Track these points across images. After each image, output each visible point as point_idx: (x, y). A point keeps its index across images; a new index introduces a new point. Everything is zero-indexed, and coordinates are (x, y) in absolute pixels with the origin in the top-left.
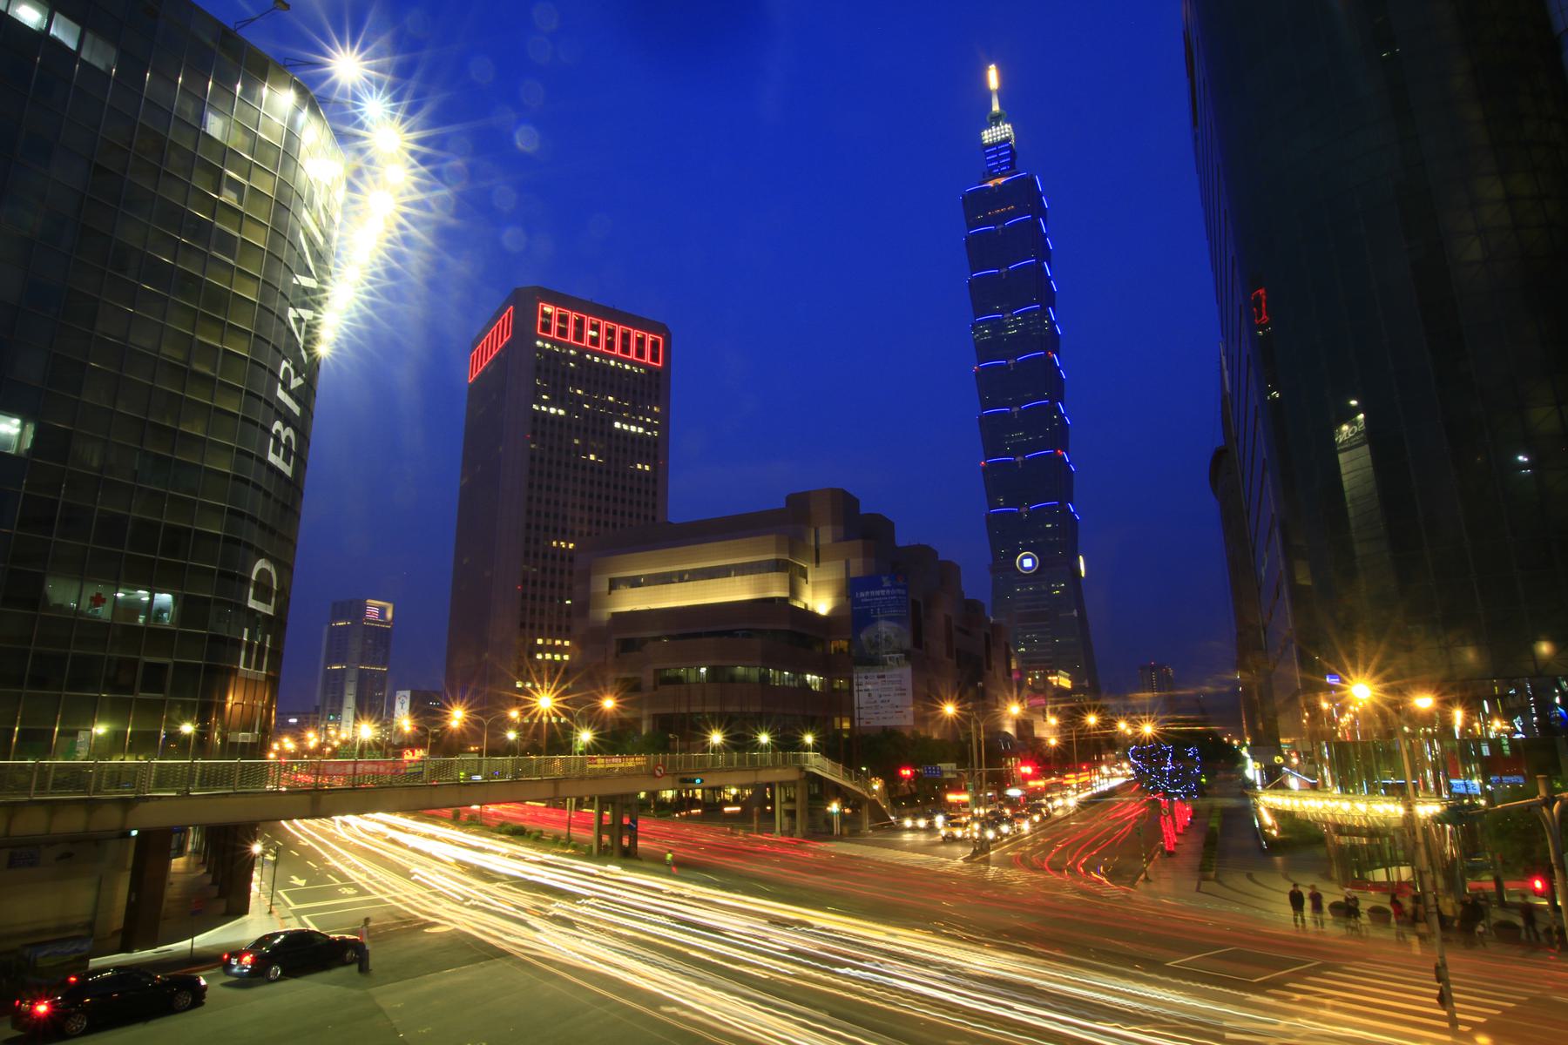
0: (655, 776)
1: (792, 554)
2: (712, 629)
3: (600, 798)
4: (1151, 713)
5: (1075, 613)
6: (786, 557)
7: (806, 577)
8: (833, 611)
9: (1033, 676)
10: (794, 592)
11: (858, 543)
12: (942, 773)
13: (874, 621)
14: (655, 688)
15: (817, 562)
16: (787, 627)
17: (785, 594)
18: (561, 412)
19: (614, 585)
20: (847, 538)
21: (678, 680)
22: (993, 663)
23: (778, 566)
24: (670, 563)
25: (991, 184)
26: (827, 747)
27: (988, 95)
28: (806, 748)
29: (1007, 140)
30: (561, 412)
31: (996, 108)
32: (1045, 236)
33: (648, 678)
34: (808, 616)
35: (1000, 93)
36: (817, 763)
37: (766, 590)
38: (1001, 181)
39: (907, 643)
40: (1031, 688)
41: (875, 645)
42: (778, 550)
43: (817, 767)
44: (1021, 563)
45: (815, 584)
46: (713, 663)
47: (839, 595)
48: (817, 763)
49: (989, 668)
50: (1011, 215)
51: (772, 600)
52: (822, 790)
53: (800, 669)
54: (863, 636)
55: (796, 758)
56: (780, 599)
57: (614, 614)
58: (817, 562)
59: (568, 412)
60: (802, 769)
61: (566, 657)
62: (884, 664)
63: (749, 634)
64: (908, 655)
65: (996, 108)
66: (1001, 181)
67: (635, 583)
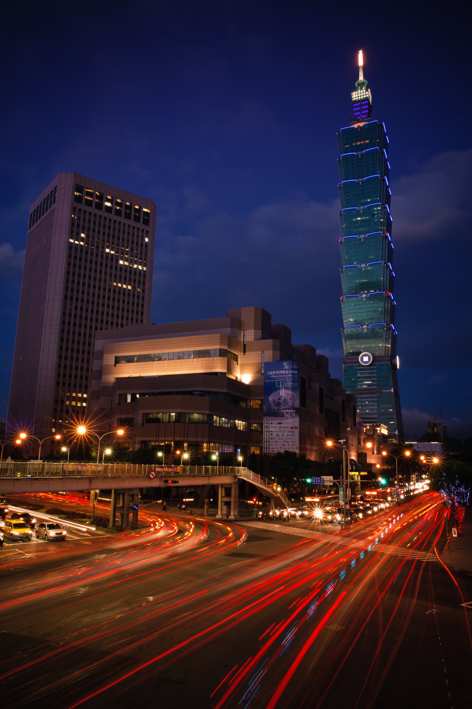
0: (150, 478)
1: (229, 346)
2: (180, 390)
3: (115, 490)
4: (423, 466)
5: (392, 390)
6: (226, 348)
7: (237, 360)
8: (253, 382)
9: (366, 427)
10: (230, 369)
11: (270, 342)
12: (324, 481)
13: (279, 389)
14: (143, 425)
15: (244, 352)
16: (225, 391)
17: (224, 371)
18: (129, 287)
19: (118, 360)
20: (263, 338)
21: (157, 421)
22: (346, 418)
23: (223, 353)
24: (154, 348)
25: (356, 126)
26: (251, 463)
27: (357, 69)
28: (238, 464)
29: (367, 99)
30: (129, 287)
31: (361, 78)
32: (385, 134)
33: (139, 419)
34: (238, 384)
35: (364, 68)
36: (245, 474)
37: (211, 367)
38: (361, 124)
39: (297, 404)
40: (366, 434)
41: (279, 404)
42: (221, 344)
43: (245, 476)
44: (362, 359)
45: (243, 366)
46: (179, 411)
47: (259, 372)
48: (245, 474)
49: (344, 420)
50: (367, 146)
51: (216, 374)
52: (246, 490)
53: (232, 416)
54: (270, 398)
55: (233, 471)
56: (221, 373)
57: (117, 379)
58: (244, 352)
59: (134, 288)
60: (235, 477)
61: (84, 404)
62: (283, 416)
63: (203, 394)
64: (298, 411)
65: (361, 78)
66: (361, 124)
67: (130, 360)
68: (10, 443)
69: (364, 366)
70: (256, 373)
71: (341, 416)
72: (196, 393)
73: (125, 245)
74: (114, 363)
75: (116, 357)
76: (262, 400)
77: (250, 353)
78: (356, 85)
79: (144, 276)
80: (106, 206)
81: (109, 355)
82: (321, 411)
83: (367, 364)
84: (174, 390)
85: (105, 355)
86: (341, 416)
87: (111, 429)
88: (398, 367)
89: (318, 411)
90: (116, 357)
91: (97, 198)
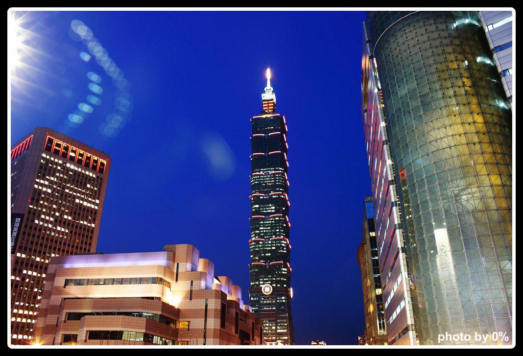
2: (121, 311)
19: (67, 282)
22: (255, 337)
68: (495, 309)
69: (265, 295)
70: (183, 299)
71: (251, 335)
72: (135, 314)
73: (76, 218)
74: (63, 285)
75: (66, 280)
76: (189, 322)
77: (181, 282)
78: (265, 89)
79: (92, 232)
80: (71, 156)
81: (61, 278)
82: (236, 332)
83: (271, 292)
84: (116, 311)
85: (56, 278)
86: (251, 335)
87: (475, 96)
88: (292, 297)
89: (234, 330)
90: (66, 280)
91: (64, 149)
